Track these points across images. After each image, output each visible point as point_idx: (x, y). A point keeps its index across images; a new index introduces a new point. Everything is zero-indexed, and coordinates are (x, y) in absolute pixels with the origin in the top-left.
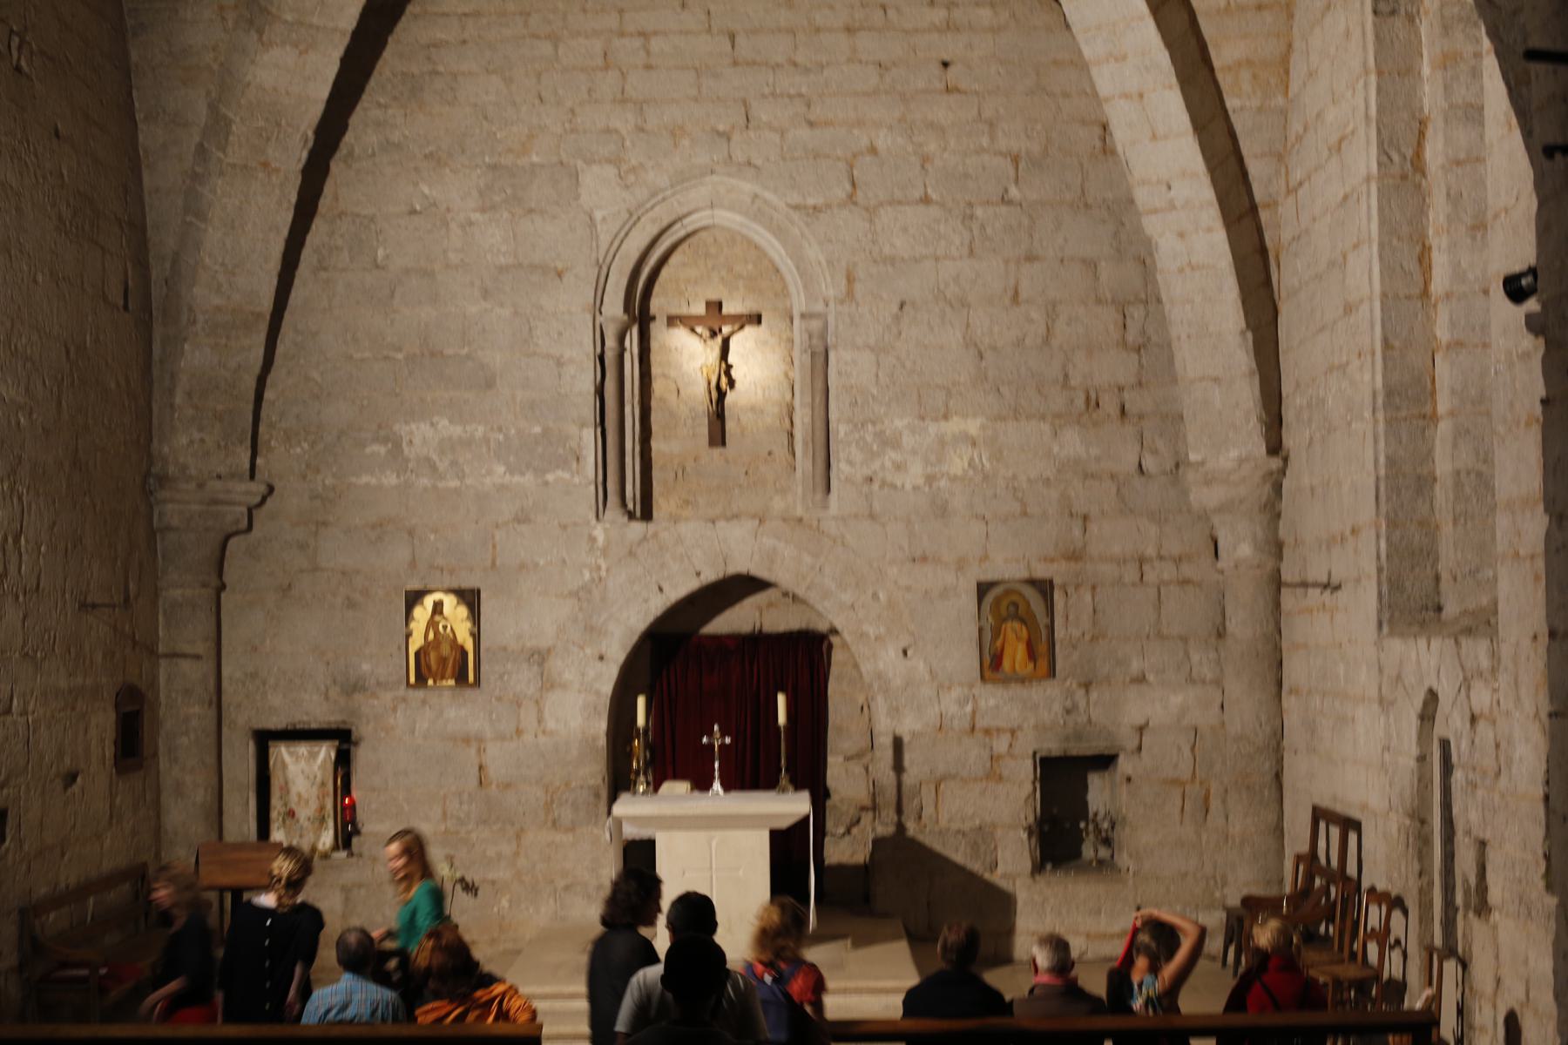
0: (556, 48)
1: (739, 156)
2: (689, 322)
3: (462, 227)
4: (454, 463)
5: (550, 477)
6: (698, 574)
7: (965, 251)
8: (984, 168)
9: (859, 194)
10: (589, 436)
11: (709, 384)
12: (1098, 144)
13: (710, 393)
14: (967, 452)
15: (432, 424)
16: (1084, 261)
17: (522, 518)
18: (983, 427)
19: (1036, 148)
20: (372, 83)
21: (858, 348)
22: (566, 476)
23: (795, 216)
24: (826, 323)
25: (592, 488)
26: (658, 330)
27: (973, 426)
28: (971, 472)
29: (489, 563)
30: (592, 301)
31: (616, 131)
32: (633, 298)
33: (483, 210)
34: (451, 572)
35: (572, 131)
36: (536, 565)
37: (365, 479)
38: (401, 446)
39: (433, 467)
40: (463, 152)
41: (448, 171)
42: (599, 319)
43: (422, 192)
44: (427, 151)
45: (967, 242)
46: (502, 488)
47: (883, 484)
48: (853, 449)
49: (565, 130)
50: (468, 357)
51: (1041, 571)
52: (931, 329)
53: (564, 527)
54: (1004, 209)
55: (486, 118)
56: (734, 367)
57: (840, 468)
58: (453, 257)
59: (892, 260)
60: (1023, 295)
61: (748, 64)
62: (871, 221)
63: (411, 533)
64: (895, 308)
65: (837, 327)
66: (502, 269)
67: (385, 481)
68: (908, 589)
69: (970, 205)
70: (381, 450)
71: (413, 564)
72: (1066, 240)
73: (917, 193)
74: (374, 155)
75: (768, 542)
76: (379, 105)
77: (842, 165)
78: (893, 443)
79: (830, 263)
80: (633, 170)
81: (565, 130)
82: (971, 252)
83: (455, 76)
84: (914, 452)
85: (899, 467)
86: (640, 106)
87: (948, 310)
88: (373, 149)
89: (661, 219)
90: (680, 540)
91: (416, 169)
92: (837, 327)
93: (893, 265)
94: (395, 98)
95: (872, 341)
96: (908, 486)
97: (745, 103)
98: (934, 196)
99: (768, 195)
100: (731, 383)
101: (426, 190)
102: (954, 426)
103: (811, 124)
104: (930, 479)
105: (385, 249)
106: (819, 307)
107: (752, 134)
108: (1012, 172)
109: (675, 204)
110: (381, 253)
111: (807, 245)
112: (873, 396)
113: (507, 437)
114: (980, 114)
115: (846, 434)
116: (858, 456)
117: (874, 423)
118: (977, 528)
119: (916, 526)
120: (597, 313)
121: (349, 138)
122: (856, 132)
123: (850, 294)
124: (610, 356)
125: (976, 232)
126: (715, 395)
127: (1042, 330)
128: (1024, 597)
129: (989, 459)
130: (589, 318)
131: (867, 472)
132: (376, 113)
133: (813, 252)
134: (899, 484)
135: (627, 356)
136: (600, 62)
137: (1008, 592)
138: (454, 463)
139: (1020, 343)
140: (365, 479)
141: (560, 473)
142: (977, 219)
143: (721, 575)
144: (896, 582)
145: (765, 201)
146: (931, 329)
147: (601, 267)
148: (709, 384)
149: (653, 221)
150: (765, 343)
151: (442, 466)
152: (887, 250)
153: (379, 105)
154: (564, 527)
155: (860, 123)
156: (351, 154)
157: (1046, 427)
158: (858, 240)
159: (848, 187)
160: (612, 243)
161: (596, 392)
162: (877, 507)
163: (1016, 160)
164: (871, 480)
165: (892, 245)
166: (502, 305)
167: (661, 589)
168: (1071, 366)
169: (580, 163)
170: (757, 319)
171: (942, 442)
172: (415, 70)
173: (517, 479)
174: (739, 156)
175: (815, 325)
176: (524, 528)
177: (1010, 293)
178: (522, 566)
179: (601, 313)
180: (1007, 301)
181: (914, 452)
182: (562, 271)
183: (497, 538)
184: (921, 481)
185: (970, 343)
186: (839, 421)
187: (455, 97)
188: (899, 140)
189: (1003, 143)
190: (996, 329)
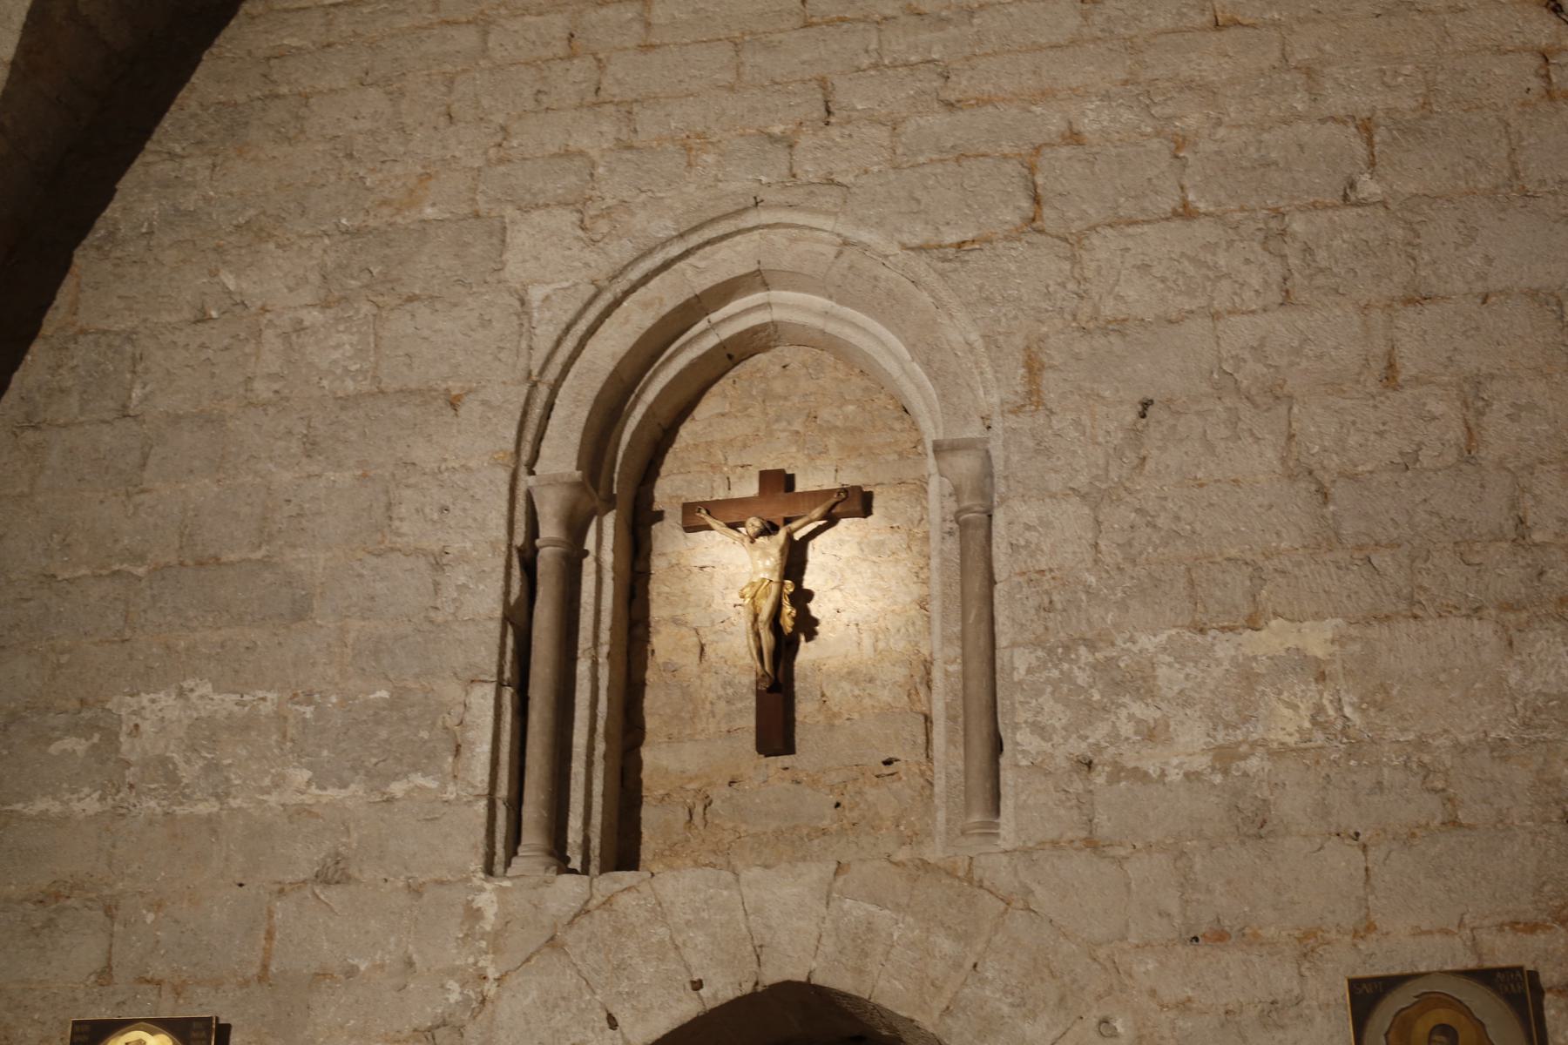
0: (485, 34)
1: (809, 170)
2: (730, 514)
3: (285, 336)
4: (213, 767)
5: (397, 788)
6: (697, 985)
7: (1275, 296)
8: (1301, 147)
9: (1047, 212)
10: (482, 700)
11: (756, 616)
12: (1536, 84)
13: (757, 635)
14: (1307, 694)
15: (181, 693)
16: (1533, 294)
17: (334, 874)
18: (1340, 640)
19: (1407, 103)
20: (166, 123)
21: (1053, 496)
22: (431, 784)
23: (920, 264)
24: (988, 456)
25: (481, 806)
26: (668, 540)
27: (1316, 639)
28: (1319, 738)
29: (254, 970)
30: (511, 447)
31: (581, 153)
32: (606, 467)
33: (325, 305)
34: (177, 991)
35: (501, 161)
36: (351, 972)
37: (41, 805)
38: (117, 735)
39: (172, 779)
40: (303, 213)
41: (271, 246)
42: (526, 481)
43: (224, 286)
44: (241, 220)
45: (1276, 277)
46: (303, 812)
47: (1118, 772)
48: (1047, 701)
49: (488, 160)
50: (266, 563)
51: (1503, 952)
52: (1210, 447)
53: (415, 891)
54: (1350, 214)
55: (350, 156)
56: (816, 598)
57: (1021, 742)
58: (262, 390)
59: (1118, 326)
60: (1407, 370)
61: (829, 23)
62: (1074, 260)
63: (109, 912)
64: (1131, 416)
65: (1007, 459)
66: (345, 402)
67: (77, 807)
68: (1184, 1006)
69: (1278, 214)
70: (77, 745)
71: (105, 975)
72: (1489, 260)
73: (1168, 203)
74: (151, 233)
75: (857, 909)
76: (172, 156)
77: (1011, 168)
78: (1140, 683)
79: (988, 339)
80: (607, 213)
81: (488, 160)
82: (1287, 299)
83: (305, 98)
84: (1184, 700)
85: (1151, 734)
86: (627, 112)
87: (1245, 409)
88: (151, 225)
89: (661, 300)
90: (660, 912)
91: (218, 249)
92: (1007, 459)
93: (1122, 334)
94: (200, 142)
95: (1082, 481)
96: (1175, 776)
97: (823, 83)
98: (1202, 206)
99: (864, 236)
100: (807, 625)
101: (231, 282)
102: (1273, 640)
103: (950, 106)
104: (1225, 757)
105: (145, 385)
106: (974, 431)
107: (834, 132)
108: (1361, 150)
109: (690, 273)
110: (137, 393)
111: (946, 321)
112: (1088, 590)
113: (320, 712)
114: (1284, 58)
115: (1029, 671)
116: (1056, 715)
117: (1092, 646)
118: (1342, 861)
119: (1198, 864)
120: (523, 470)
121: (113, 211)
122: (1038, 110)
123: (1033, 396)
124: (547, 558)
125: (1294, 261)
126: (767, 639)
127: (1456, 433)
128: (1467, 1012)
129: (1356, 707)
130: (503, 476)
131: (1081, 748)
132: (166, 168)
133: (960, 330)
134: (1153, 771)
135: (589, 565)
136: (560, 48)
137: (1429, 1001)
138: (213, 767)
139: (1407, 462)
140: (41, 805)
141: (418, 779)
142: (1294, 237)
143: (747, 988)
144: (1153, 993)
145: (865, 248)
146: (1210, 447)
147: (534, 385)
148: (756, 616)
149: (646, 305)
150: (879, 547)
151: (187, 773)
152: (1109, 309)
153: (172, 156)
154: (415, 891)
155: (1046, 95)
156: (111, 234)
157: (1484, 630)
158: (1048, 295)
159: (1026, 204)
160: (558, 343)
161: (507, 619)
162: (1105, 825)
163: (1366, 128)
164: (1089, 764)
165: (1119, 298)
166: (339, 465)
167: (612, 1022)
168: (1528, 501)
169: (510, 212)
170: (859, 502)
171: (1247, 676)
172: (241, 98)
173: (332, 793)
174: (809, 170)
175: (965, 464)
176: (333, 895)
177: (1378, 367)
178: (322, 975)
179: (532, 473)
180: (1372, 386)
181: (1184, 700)
182: (458, 397)
183: (278, 916)
184: (1201, 763)
185: (1297, 470)
186: (1014, 644)
187: (302, 132)
188: (1127, 115)
189: (1336, 102)
190: (1352, 441)
